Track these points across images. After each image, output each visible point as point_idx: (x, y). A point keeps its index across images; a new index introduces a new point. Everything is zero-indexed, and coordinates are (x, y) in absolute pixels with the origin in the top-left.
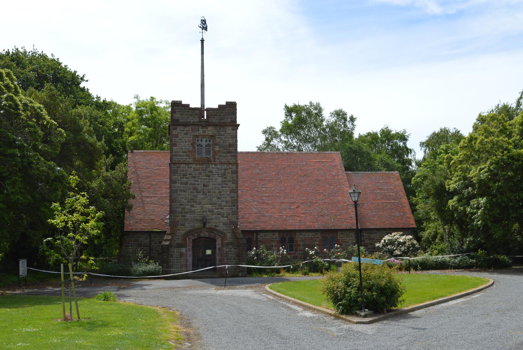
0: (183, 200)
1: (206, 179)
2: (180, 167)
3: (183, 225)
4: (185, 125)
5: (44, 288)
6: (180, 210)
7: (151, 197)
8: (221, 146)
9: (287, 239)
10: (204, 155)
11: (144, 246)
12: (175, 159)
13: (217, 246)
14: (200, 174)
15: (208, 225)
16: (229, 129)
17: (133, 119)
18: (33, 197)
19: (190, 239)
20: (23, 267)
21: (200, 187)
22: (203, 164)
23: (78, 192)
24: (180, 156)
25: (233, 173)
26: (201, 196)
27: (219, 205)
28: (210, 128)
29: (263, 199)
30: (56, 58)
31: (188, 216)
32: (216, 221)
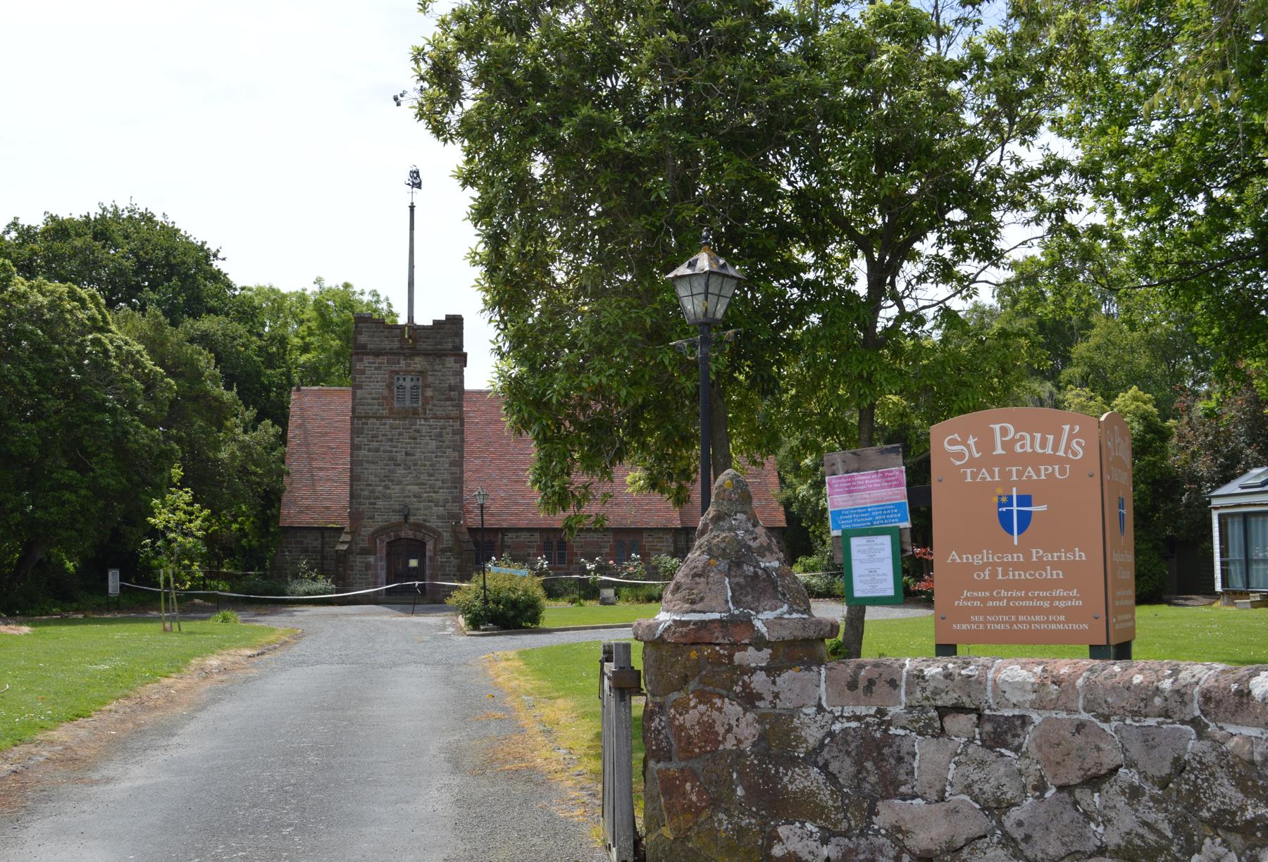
0: (372, 478)
1: (410, 443)
4: (377, 354)
5: (146, 612)
6: (366, 493)
7: (328, 469)
8: (435, 389)
9: (555, 543)
10: (408, 404)
13: (428, 554)
14: (401, 434)
15: (412, 519)
16: (450, 362)
17: (309, 320)
19: (382, 541)
20: (114, 580)
21: (400, 457)
22: (404, 418)
23: (181, 488)
24: (368, 404)
25: (454, 433)
26: (401, 471)
27: (431, 486)
28: (417, 359)
30: (170, 220)
31: (380, 504)
32: (426, 512)
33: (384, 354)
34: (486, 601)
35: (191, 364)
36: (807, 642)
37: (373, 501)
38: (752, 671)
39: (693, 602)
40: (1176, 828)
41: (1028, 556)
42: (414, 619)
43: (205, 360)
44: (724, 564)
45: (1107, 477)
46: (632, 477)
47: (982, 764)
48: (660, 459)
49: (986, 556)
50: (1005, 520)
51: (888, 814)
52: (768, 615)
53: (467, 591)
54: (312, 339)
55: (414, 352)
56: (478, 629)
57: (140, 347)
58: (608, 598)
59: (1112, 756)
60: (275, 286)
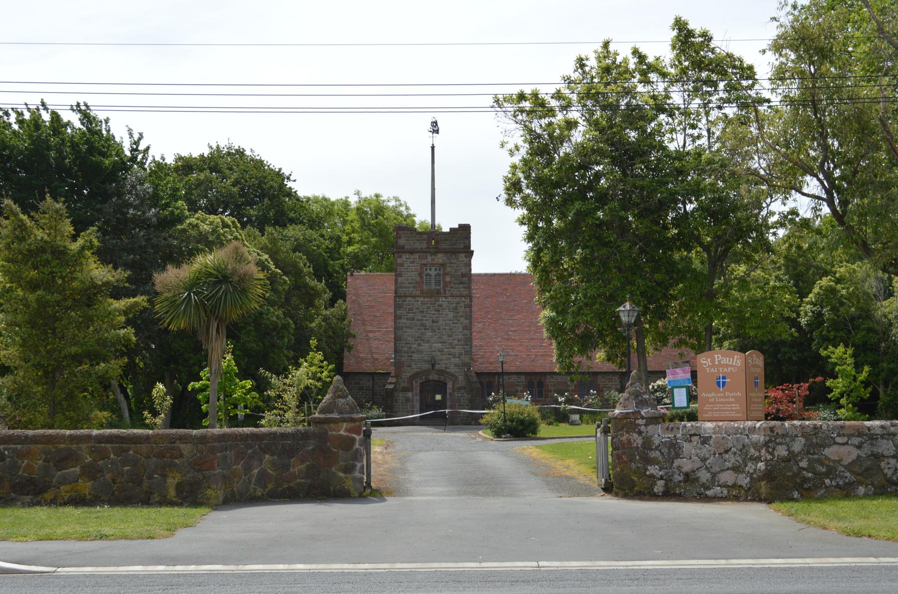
1: (435, 314)
2: (405, 301)
3: (409, 366)
4: (412, 252)
6: (405, 349)
7: (375, 332)
9: (536, 383)
10: (433, 286)
11: (366, 390)
12: (400, 291)
13: (448, 391)
14: (428, 308)
15: (437, 367)
16: (462, 257)
18: (264, 344)
19: (417, 382)
21: (428, 323)
22: (431, 297)
24: (406, 287)
25: (465, 306)
27: (450, 344)
28: (439, 256)
29: (508, 335)
31: (415, 356)
32: (447, 362)
33: (416, 253)
34: (505, 421)
35: (295, 265)
36: (656, 418)
37: (410, 354)
38: (641, 425)
39: (625, 407)
40: (743, 461)
41: (725, 394)
42: (446, 434)
43: (301, 259)
44: (633, 397)
45: (748, 371)
46: (600, 355)
47: (700, 449)
48: (611, 348)
49: (713, 394)
50: (718, 383)
51: (677, 462)
52: (645, 411)
53: (492, 415)
54: (355, 235)
55: (437, 251)
56: (501, 438)
57: (266, 256)
58: (576, 421)
59: (730, 445)
60: (327, 196)
